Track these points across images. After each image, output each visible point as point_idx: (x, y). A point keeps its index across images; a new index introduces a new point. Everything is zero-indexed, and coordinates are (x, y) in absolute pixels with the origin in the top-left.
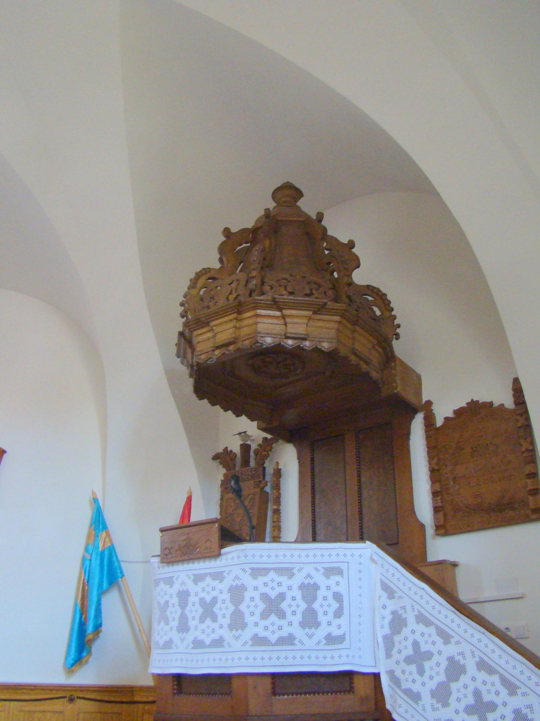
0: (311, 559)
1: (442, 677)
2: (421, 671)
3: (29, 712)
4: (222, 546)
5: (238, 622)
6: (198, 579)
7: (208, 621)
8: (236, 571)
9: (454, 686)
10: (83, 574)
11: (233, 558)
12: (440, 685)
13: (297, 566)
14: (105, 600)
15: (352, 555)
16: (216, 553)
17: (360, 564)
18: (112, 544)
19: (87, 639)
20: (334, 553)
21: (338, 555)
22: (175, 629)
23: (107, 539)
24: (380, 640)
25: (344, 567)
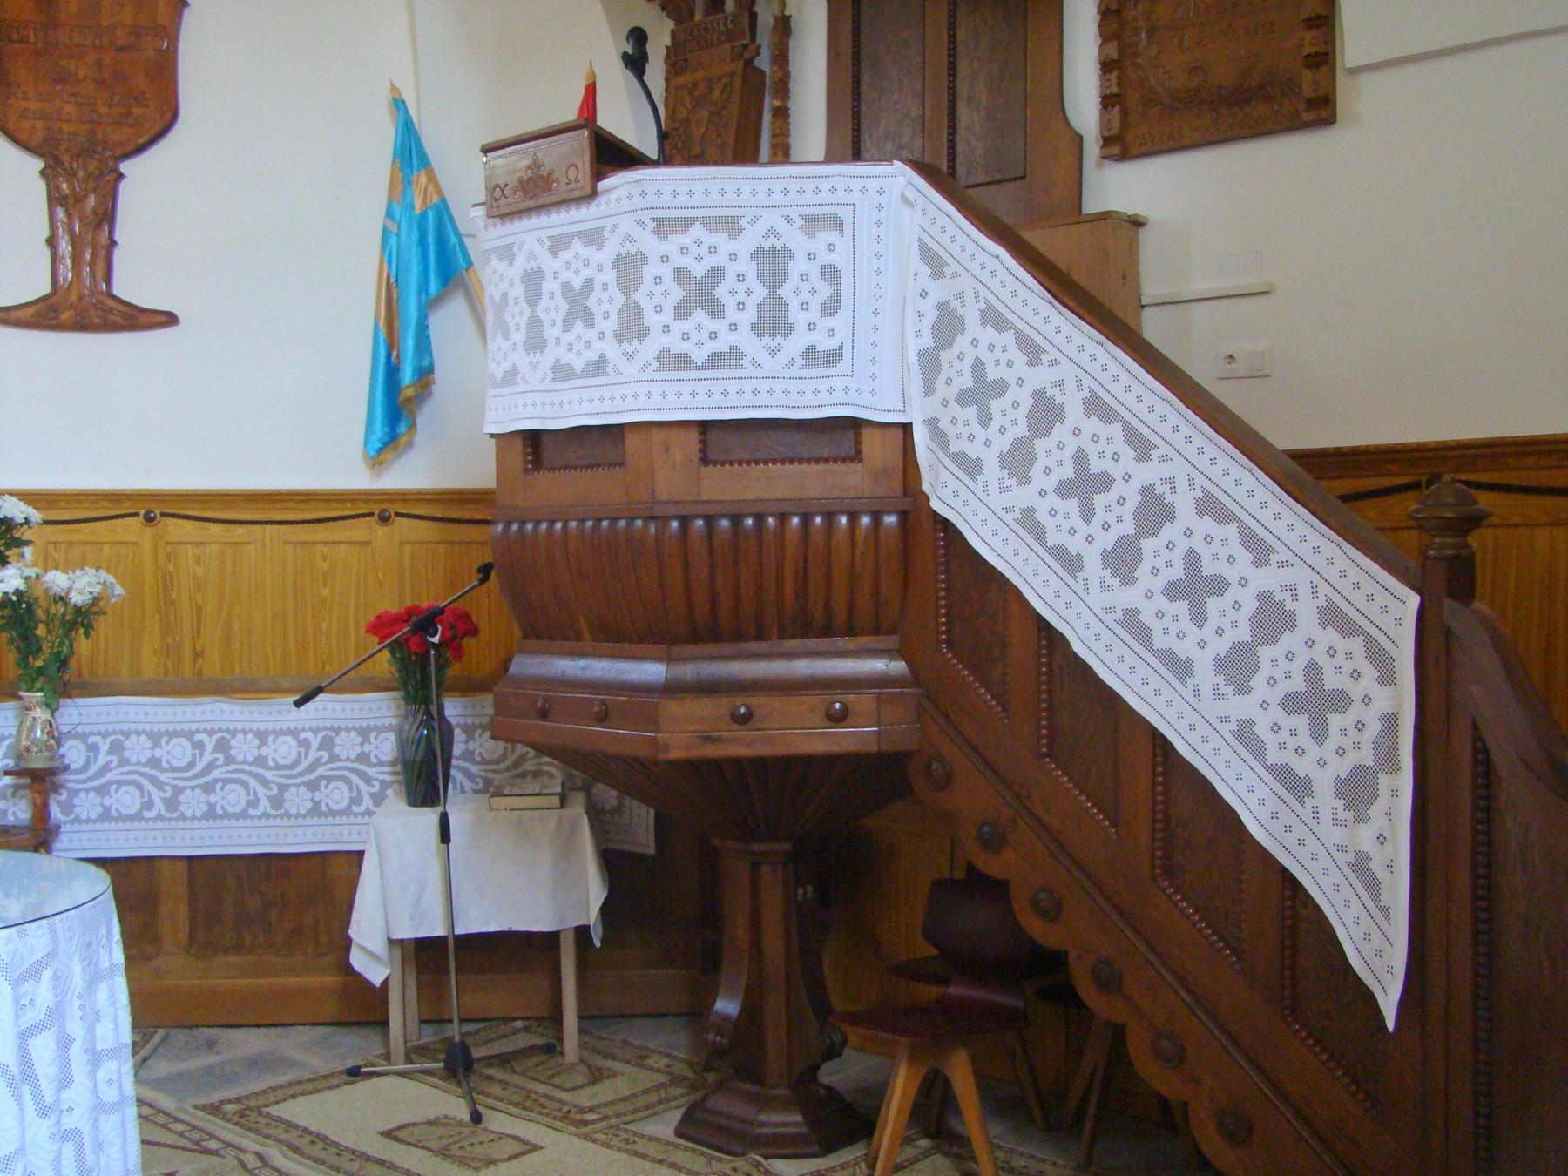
0: (778, 198)
1: (1021, 430)
2: (985, 419)
3: (304, 543)
4: (598, 176)
5: (631, 326)
6: (558, 244)
7: (579, 326)
8: (627, 224)
9: (1041, 445)
10: (386, 265)
11: (619, 200)
12: (1017, 443)
13: (749, 214)
14: (436, 322)
15: (864, 190)
16: (588, 190)
17: (880, 208)
18: (443, 199)
19: (402, 398)
20: (825, 185)
21: (833, 190)
22: (520, 346)
23: (430, 189)
24: (913, 359)
25: (845, 214)
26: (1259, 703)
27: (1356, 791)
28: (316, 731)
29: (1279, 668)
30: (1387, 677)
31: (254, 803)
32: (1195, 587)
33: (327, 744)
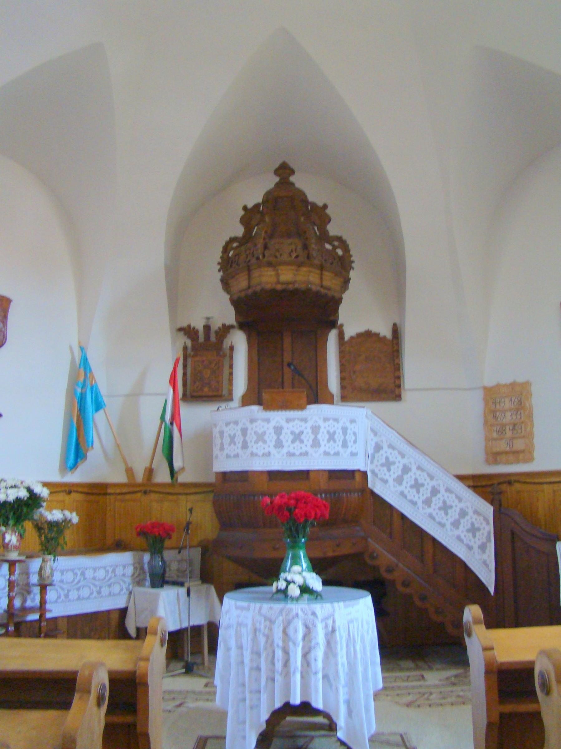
6: (288, 421)
26: (462, 531)
27: (483, 547)
28: (79, 569)
29: (465, 524)
30: (488, 523)
31: (92, 593)
32: (445, 508)
33: (114, 571)
